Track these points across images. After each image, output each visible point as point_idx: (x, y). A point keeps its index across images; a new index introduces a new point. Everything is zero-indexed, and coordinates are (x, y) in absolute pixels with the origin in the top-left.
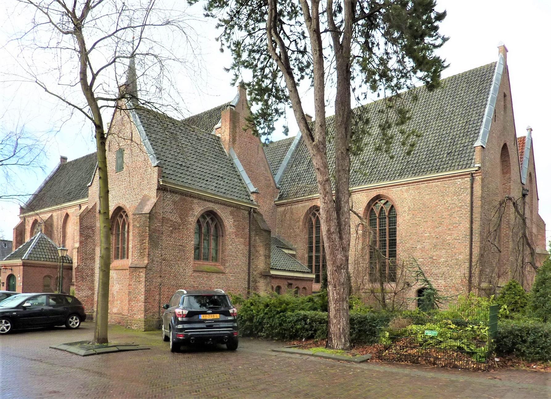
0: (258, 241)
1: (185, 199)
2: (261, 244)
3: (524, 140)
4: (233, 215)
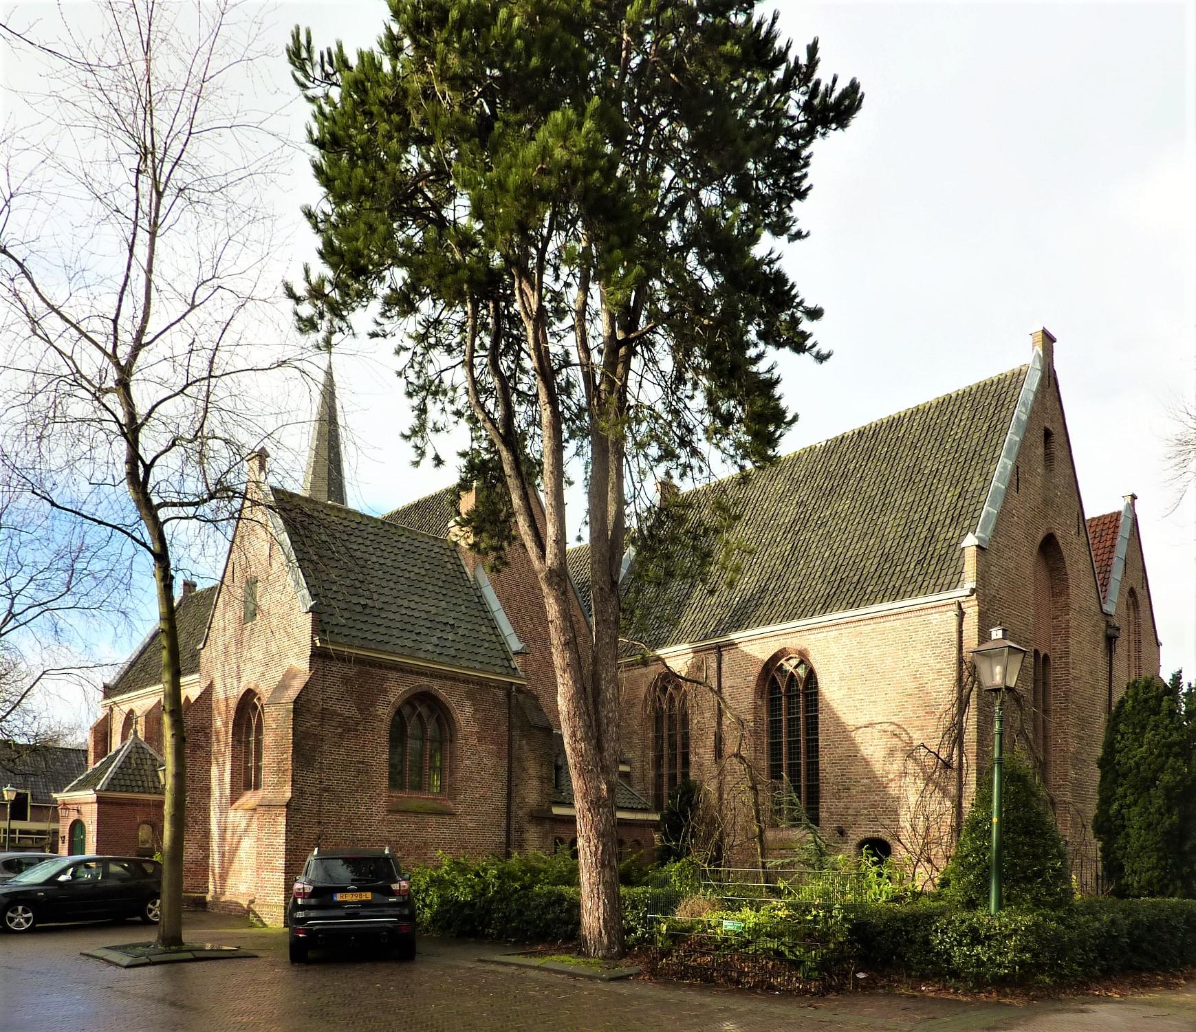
0: (526, 748)
1: (368, 673)
2: (531, 755)
3: (1117, 520)
4: (472, 700)
